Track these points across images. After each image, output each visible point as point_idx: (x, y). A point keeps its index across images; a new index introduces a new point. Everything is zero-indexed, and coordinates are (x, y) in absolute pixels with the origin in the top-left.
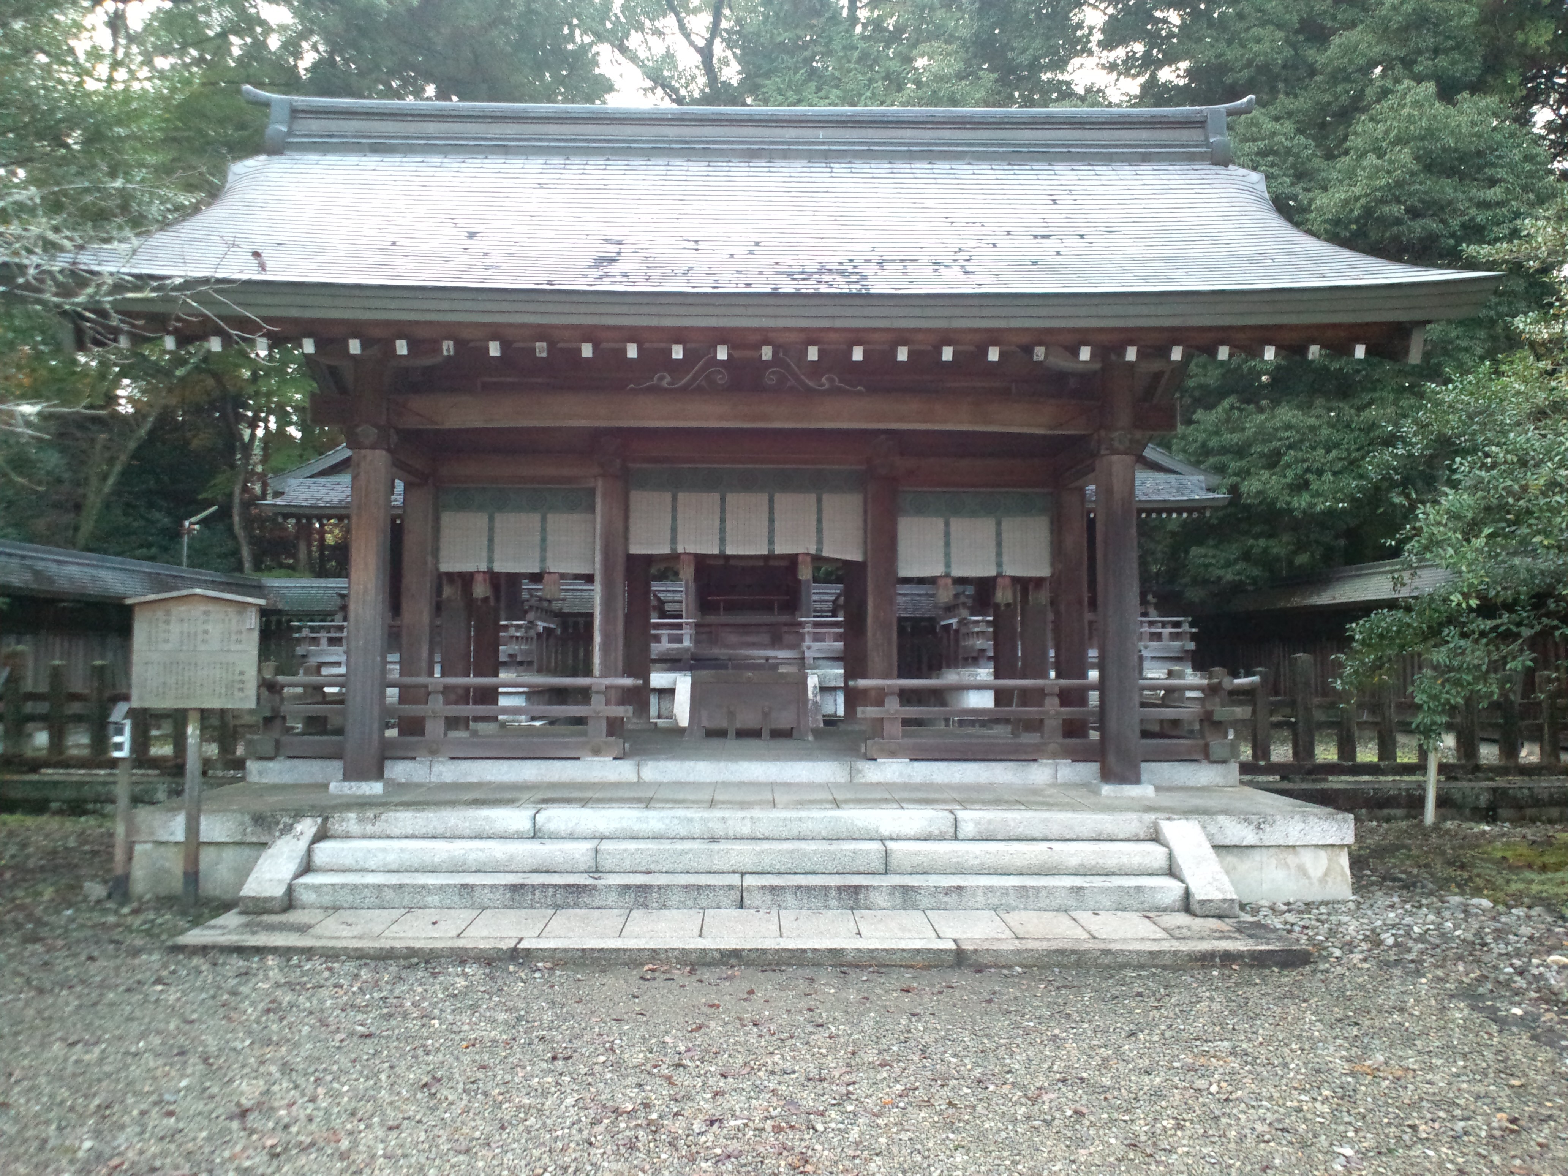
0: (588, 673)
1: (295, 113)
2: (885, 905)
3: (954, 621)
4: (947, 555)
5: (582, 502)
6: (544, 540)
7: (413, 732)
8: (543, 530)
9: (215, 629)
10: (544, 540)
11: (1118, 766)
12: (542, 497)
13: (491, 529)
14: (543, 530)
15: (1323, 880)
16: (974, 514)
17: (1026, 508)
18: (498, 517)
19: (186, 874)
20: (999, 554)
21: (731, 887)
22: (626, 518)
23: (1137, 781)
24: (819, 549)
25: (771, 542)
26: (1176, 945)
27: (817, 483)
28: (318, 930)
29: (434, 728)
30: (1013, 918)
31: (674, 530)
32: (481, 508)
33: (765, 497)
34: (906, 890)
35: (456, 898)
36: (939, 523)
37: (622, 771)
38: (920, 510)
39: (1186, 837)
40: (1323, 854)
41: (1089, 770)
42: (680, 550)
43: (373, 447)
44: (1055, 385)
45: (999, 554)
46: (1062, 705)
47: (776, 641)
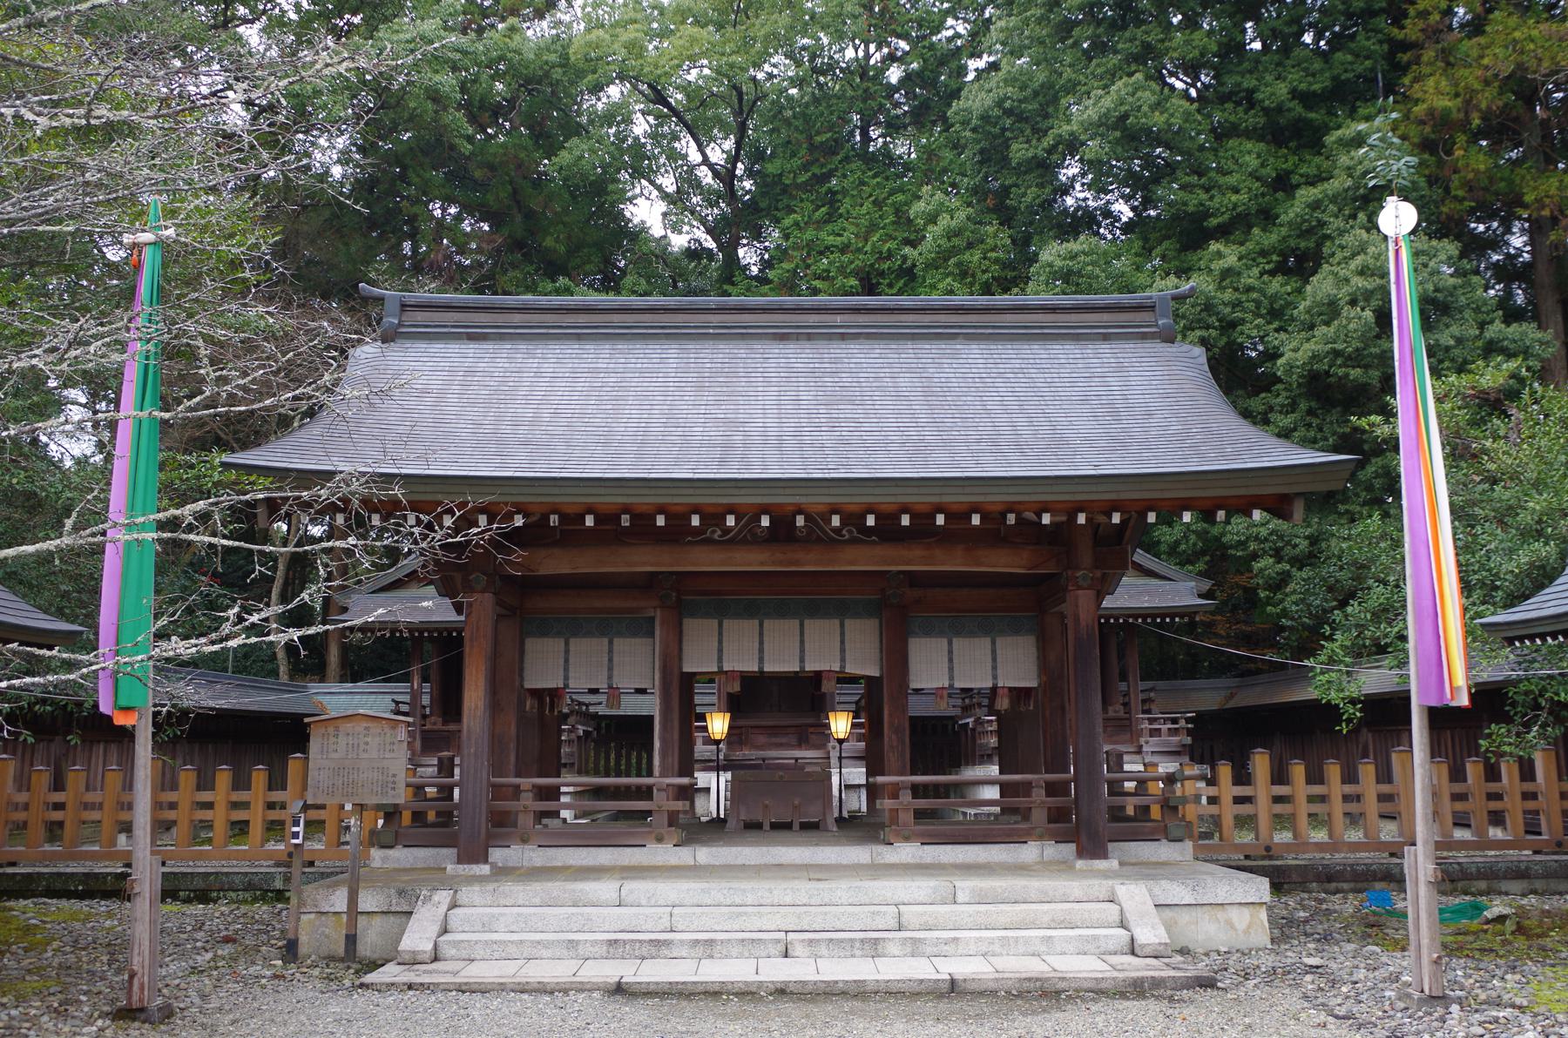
0: (650, 774)
1: (404, 307)
2: (897, 953)
3: (970, 720)
4: (951, 669)
5: (644, 628)
6: (610, 660)
7: (501, 826)
8: (611, 651)
9: (374, 741)
10: (610, 660)
11: (1091, 846)
12: (607, 626)
13: (567, 652)
14: (611, 651)
15: (1247, 932)
16: (972, 634)
17: (1015, 629)
18: (572, 641)
19: (347, 936)
20: (994, 668)
21: (778, 941)
22: (680, 642)
23: (1105, 856)
24: (843, 667)
25: (802, 660)
26: (1116, 974)
27: (842, 611)
28: (463, 973)
29: (525, 821)
30: (996, 961)
31: (720, 651)
32: (558, 634)
33: (797, 622)
34: (915, 941)
35: (565, 952)
36: (943, 643)
37: (684, 855)
38: (928, 632)
39: (1135, 895)
40: (1246, 911)
41: (1069, 849)
42: (863, 782)
43: (483, 591)
44: (1029, 533)
45: (994, 668)
46: (1048, 795)
47: (803, 742)
